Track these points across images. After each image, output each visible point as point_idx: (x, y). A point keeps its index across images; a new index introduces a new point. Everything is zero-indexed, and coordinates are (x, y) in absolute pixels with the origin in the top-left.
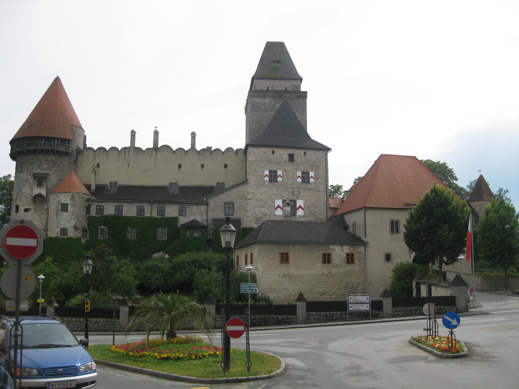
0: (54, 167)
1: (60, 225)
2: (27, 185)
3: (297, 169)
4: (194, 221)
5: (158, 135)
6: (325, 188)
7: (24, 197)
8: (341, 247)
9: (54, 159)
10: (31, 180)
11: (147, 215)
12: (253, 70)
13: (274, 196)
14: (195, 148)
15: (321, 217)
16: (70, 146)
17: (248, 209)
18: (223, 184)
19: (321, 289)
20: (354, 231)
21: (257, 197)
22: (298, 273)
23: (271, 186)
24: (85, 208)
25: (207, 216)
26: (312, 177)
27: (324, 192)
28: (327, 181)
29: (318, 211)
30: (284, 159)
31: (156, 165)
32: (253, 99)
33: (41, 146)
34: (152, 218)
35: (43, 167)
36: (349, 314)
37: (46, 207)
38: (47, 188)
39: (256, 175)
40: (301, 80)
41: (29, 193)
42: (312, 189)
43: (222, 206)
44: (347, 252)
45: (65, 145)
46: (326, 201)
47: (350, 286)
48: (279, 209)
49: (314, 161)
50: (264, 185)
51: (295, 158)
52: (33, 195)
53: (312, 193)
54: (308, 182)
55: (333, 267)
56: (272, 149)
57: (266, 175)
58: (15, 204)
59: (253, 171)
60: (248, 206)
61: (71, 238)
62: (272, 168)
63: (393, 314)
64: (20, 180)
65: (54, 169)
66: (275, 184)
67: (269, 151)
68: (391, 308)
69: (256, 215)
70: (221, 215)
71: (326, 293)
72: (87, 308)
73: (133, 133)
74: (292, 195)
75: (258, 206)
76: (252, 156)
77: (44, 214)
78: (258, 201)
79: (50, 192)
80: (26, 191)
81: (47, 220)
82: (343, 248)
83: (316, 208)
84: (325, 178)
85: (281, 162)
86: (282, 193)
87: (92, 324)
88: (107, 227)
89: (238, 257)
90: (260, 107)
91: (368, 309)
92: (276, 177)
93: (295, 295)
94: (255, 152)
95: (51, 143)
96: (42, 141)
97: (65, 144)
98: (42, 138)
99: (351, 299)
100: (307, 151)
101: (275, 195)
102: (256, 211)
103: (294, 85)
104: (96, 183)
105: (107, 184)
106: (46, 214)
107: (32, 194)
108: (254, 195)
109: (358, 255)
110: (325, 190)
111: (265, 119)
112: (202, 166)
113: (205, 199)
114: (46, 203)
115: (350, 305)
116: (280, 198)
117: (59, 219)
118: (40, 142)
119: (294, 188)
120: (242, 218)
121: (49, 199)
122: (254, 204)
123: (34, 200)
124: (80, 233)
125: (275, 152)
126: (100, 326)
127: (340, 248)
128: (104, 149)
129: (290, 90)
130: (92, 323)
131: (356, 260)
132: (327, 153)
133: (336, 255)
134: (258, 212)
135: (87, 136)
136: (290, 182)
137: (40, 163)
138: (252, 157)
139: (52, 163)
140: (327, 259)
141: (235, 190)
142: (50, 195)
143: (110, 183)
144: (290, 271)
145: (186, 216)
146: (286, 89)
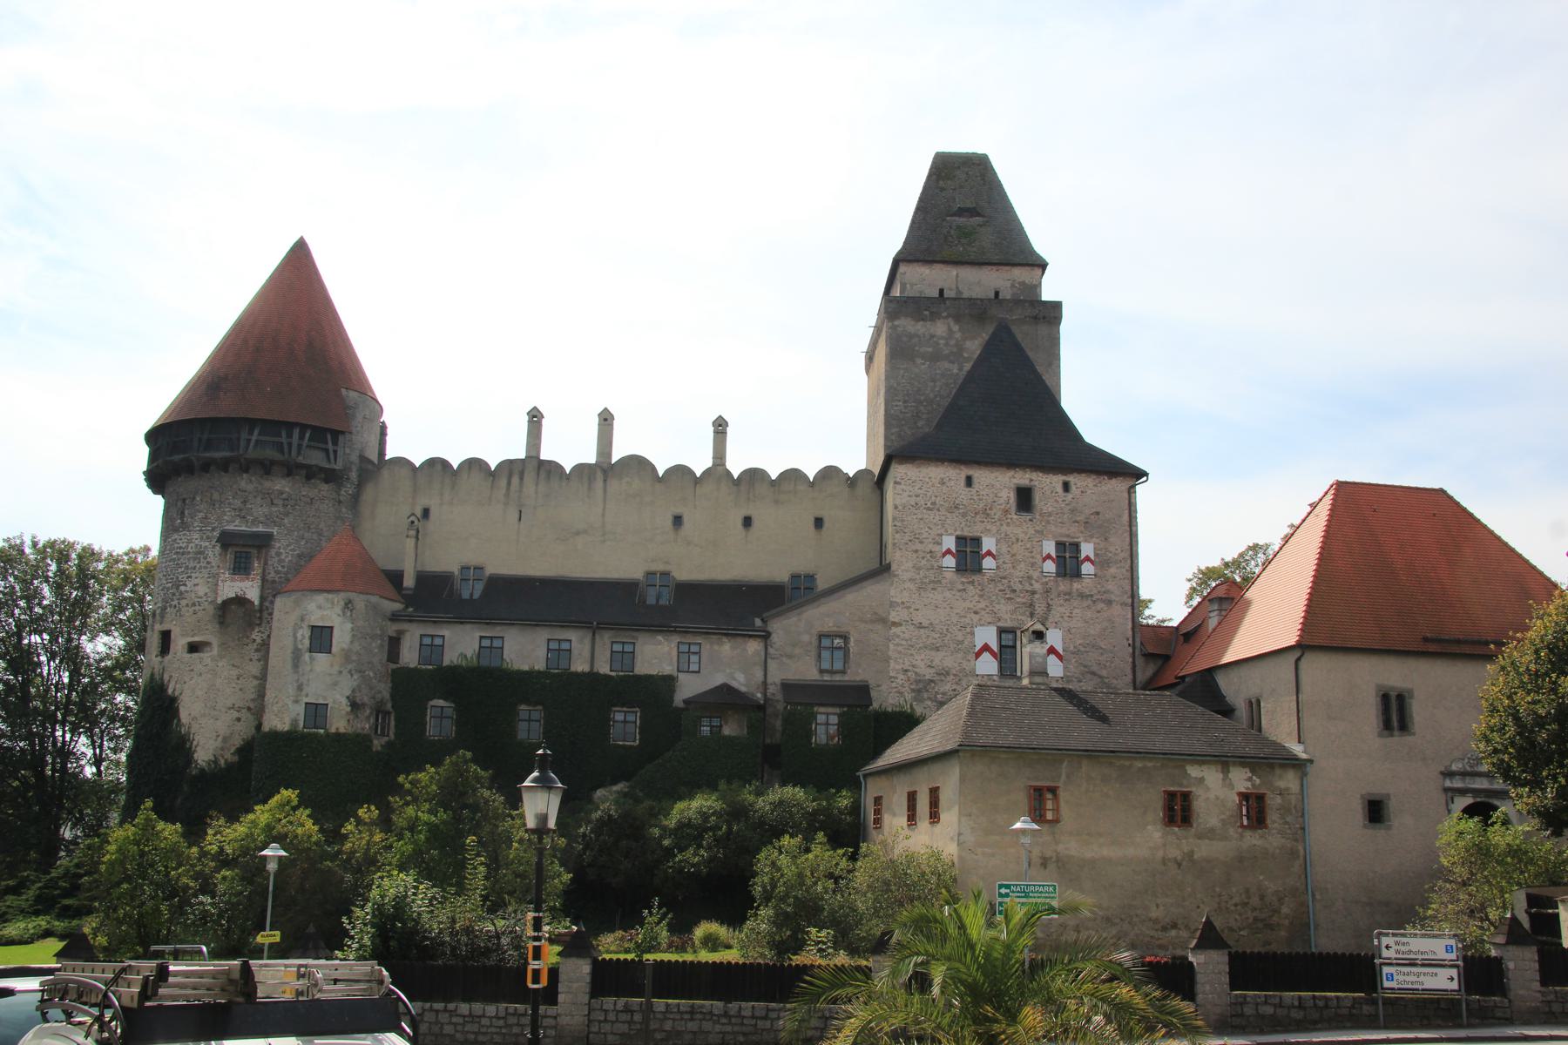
0: (287, 514)
1: (304, 693)
2: (201, 567)
3: (1041, 532)
4: (726, 689)
5: (612, 425)
6: (1130, 593)
7: (187, 605)
8: (1223, 772)
9: (287, 489)
10: (213, 553)
11: (580, 666)
12: (896, 239)
13: (973, 615)
14: (724, 465)
15: (1115, 682)
16: (340, 453)
17: (890, 653)
18: (811, 578)
19: (1162, 908)
21: (919, 617)
22: (1088, 855)
23: (963, 583)
24: (386, 644)
25: (765, 675)
26: (1087, 559)
27: (1126, 605)
28: (1135, 573)
29: (1108, 664)
30: (1002, 501)
31: (603, 515)
32: (896, 323)
33: (247, 448)
34: (593, 678)
35: (252, 515)
36: (1383, 1004)
37: (259, 640)
38: (264, 580)
39: (916, 551)
40: (1042, 266)
41: (206, 594)
42: (1087, 596)
43: (811, 643)
44: (1244, 790)
45: (322, 449)
46: (1130, 633)
47: (1255, 901)
49: (1094, 510)
50: (940, 582)
51: (1037, 498)
52: (219, 601)
53: (1089, 607)
54: (1077, 574)
55: (1200, 837)
56: (965, 471)
57: (948, 552)
58: (158, 627)
60: (891, 646)
61: (338, 734)
62: (966, 529)
63: (1547, 1009)
64: (177, 553)
65: (286, 521)
66: (976, 578)
68: (1537, 985)
69: (916, 673)
70: (805, 670)
71: (1180, 922)
72: (536, 973)
73: (535, 417)
74: (1028, 613)
75: (921, 645)
76: (903, 490)
77: (251, 660)
78: (922, 630)
79: (271, 591)
80: (198, 587)
81: (263, 677)
82: (1230, 775)
83: (1102, 654)
84: (1129, 561)
85: (992, 513)
86: (998, 607)
87: (455, 1024)
88: (453, 702)
89: (878, 800)
90: (917, 348)
91: (1454, 985)
92: (978, 556)
93: (1078, 926)
94: (914, 478)
96: (251, 433)
97: (323, 446)
98: (252, 423)
99: (1390, 945)
100: (1071, 479)
101: (976, 613)
102: (915, 662)
103: (1022, 283)
104: (419, 569)
105: (453, 573)
106: (259, 660)
107: (216, 598)
108: (911, 610)
109: (1279, 800)
110: (1130, 600)
111: (932, 384)
112: (747, 522)
113: (758, 622)
114: (259, 625)
115: (1386, 970)
116: (989, 623)
117: (303, 674)
118: (244, 435)
120: (872, 683)
121: (271, 614)
122: (911, 639)
123: (220, 616)
124: (368, 718)
125: (975, 480)
126: (484, 1030)
127: (1221, 776)
128: (444, 464)
130: (454, 1020)
131: (1273, 818)
132: (1133, 487)
134: (922, 665)
135: (388, 424)
136: (1021, 574)
137: (245, 502)
139: (281, 502)
140: (1178, 810)
141: (851, 596)
142: (272, 603)
143: (463, 568)
144: (1060, 848)
145: (699, 672)
146: (997, 294)
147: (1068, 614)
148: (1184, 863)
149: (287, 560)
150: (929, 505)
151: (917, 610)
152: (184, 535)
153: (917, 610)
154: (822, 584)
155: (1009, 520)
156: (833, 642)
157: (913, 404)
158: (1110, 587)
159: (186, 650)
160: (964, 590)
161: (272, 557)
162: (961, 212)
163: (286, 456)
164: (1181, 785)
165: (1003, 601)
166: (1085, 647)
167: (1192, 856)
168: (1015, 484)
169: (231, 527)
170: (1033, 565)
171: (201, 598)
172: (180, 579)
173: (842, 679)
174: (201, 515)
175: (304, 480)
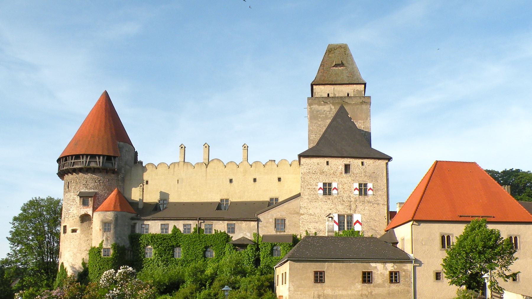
7: (71, 217)
10: (78, 199)
13: (329, 210)
17: (300, 225)
20: (403, 247)
21: (311, 212)
32: (312, 107)
39: (309, 189)
48: (358, 224)
51: (352, 168)
55: (374, 287)
56: (327, 159)
59: (306, 184)
64: (67, 200)
66: (330, 197)
67: (323, 161)
70: (271, 231)
74: (349, 209)
78: (311, 216)
82: (386, 265)
94: (308, 163)
95: (73, 159)
100: (365, 161)
101: (331, 209)
103: (357, 90)
108: (307, 209)
109: (404, 273)
116: (335, 213)
119: (351, 202)
122: (308, 219)
129: (352, 95)
133: (378, 274)
138: (305, 169)
140: (367, 278)
141: (286, 205)
146: (348, 95)
147: (363, 209)
148: (369, 296)
149: (101, 201)
150: (314, 172)
151: (310, 209)
152: (69, 194)
153: (310, 209)
154: (280, 200)
155: (342, 176)
156: (280, 223)
157: (318, 135)
158: (379, 199)
159: (71, 232)
160: (326, 201)
161: (96, 200)
162: (336, 65)
163: (98, 166)
164: (368, 269)
165: (340, 205)
166: (370, 220)
167: (372, 293)
168: (344, 163)
169: (82, 191)
170: (351, 192)
171: (75, 214)
172: (68, 208)
173: (284, 234)
174: (74, 187)
175: (106, 173)
